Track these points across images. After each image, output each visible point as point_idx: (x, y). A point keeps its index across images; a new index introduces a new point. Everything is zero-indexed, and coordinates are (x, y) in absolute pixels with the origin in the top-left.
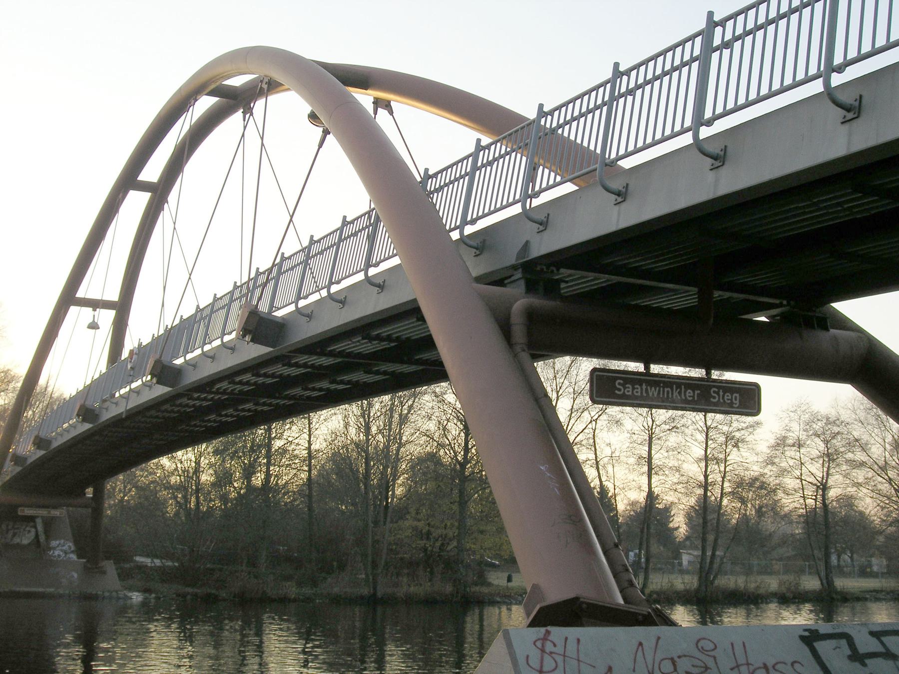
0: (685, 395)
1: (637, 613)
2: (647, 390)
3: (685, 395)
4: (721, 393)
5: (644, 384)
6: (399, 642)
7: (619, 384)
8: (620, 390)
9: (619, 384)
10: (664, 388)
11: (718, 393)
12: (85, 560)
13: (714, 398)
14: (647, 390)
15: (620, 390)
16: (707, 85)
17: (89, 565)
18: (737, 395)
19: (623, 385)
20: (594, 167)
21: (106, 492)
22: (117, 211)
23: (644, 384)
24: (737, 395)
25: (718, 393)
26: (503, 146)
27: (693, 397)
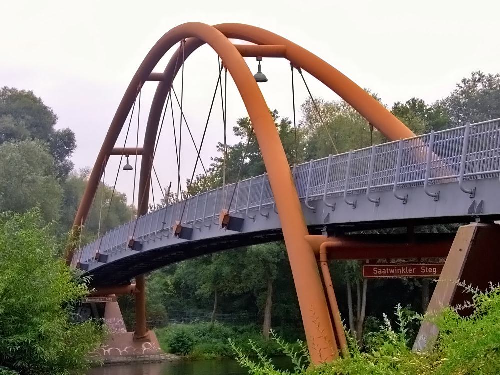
0: (408, 271)
1: (407, 127)
2: (389, 271)
3: (408, 271)
4: (427, 269)
5: (399, 307)
6: (136, 210)
7: (375, 270)
8: (376, 272)
9: (375, 270)
10: (397, 269)
11: (425, 269)
12: (133, 333)
13: (424, 271)
14: (389, 271)
15: (376, 272)
16: (370, 222)
17: (137, 337)
18: (436, 269)
19: (377, 270)
20: (322, 194)
21: (145, 303)
22: (104, 170)
23: (399, 307)
24: (436, 269)
25: (425, 269)
26: (322, 264)
27: (412, 272)
